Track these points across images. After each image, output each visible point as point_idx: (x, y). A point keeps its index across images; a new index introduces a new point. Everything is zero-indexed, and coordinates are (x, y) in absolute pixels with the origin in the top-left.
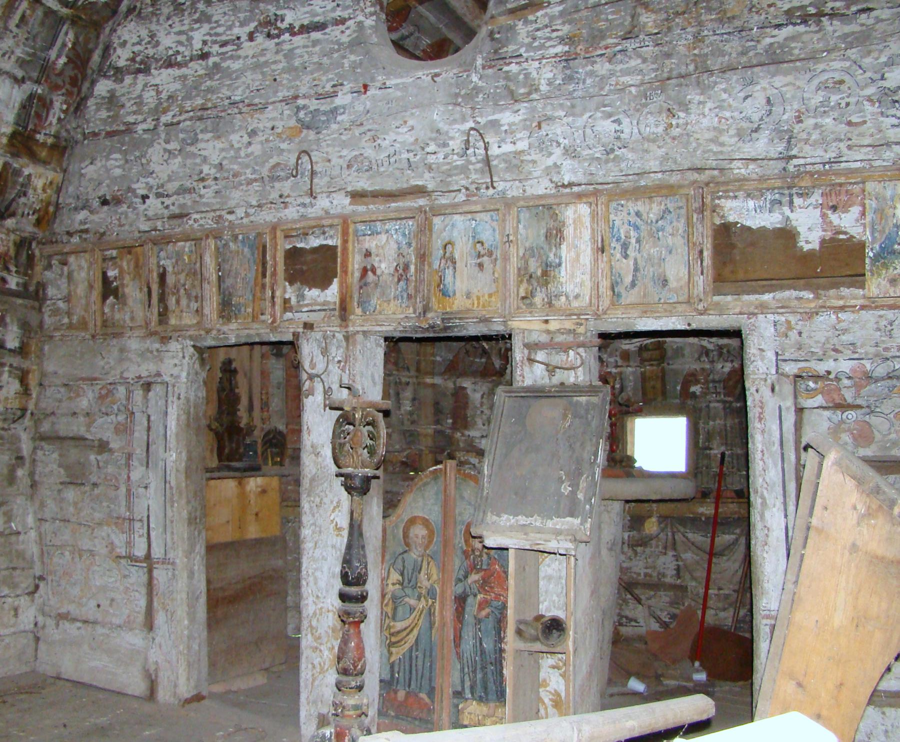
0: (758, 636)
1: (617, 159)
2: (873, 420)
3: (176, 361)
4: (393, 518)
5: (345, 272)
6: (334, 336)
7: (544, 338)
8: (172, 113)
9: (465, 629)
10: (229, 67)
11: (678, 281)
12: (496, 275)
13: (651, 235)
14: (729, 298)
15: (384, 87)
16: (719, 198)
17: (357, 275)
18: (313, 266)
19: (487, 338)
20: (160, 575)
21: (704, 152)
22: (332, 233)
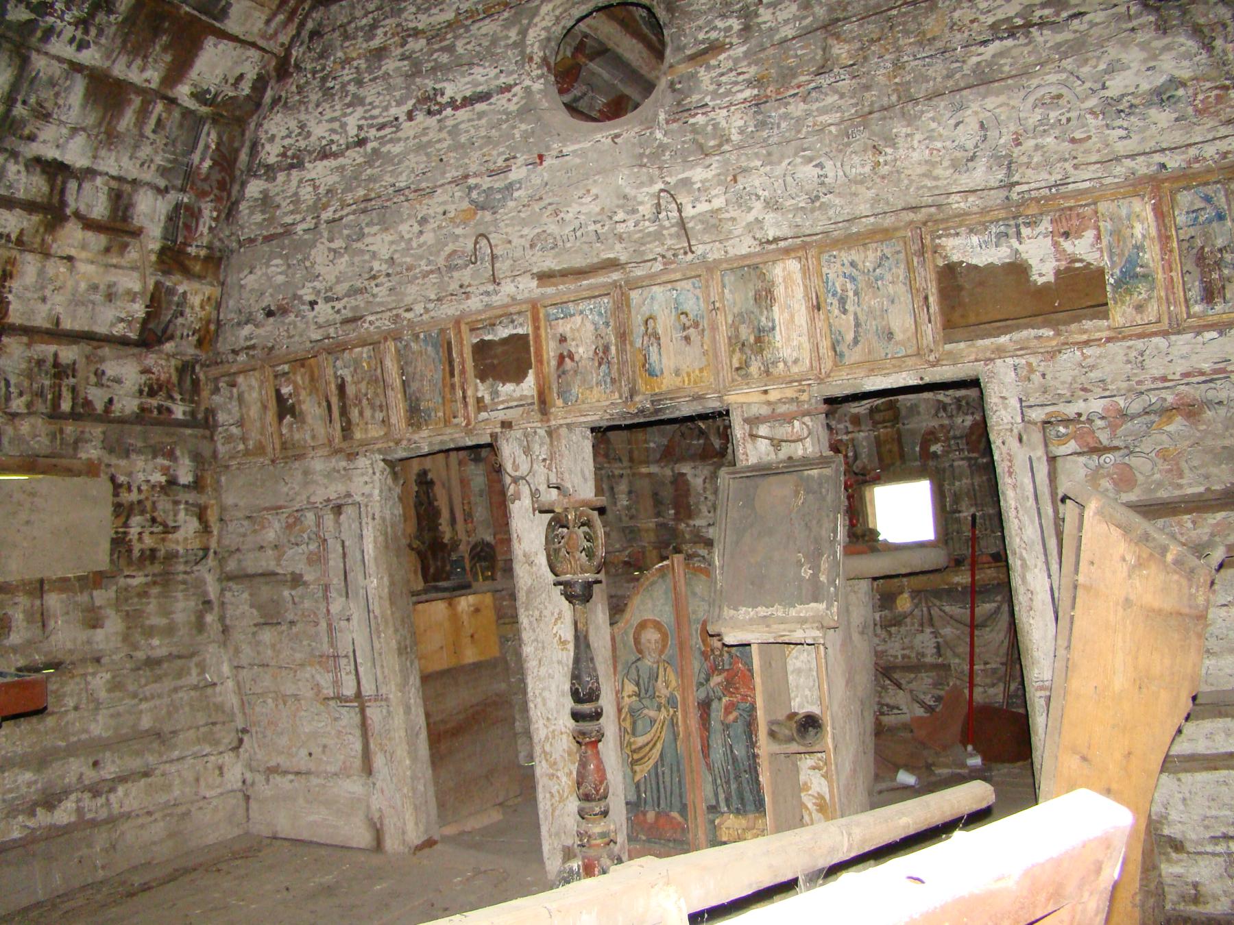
2: (1134, 461)
3: (366, 478)
4: (621, 624)
5: (540, 361)
7: (765, 411)
8: (333, 209)
9: (713, 737)
10: (389, 152)
11: (905, 331)
13: (870, 285)
14: (962, 345)
15: (561, 155)
16: (940, 237)
17: (554, 363)
18: (504, 359)
20: (374, 713)
21: (918, 189)
22: (521, 320)
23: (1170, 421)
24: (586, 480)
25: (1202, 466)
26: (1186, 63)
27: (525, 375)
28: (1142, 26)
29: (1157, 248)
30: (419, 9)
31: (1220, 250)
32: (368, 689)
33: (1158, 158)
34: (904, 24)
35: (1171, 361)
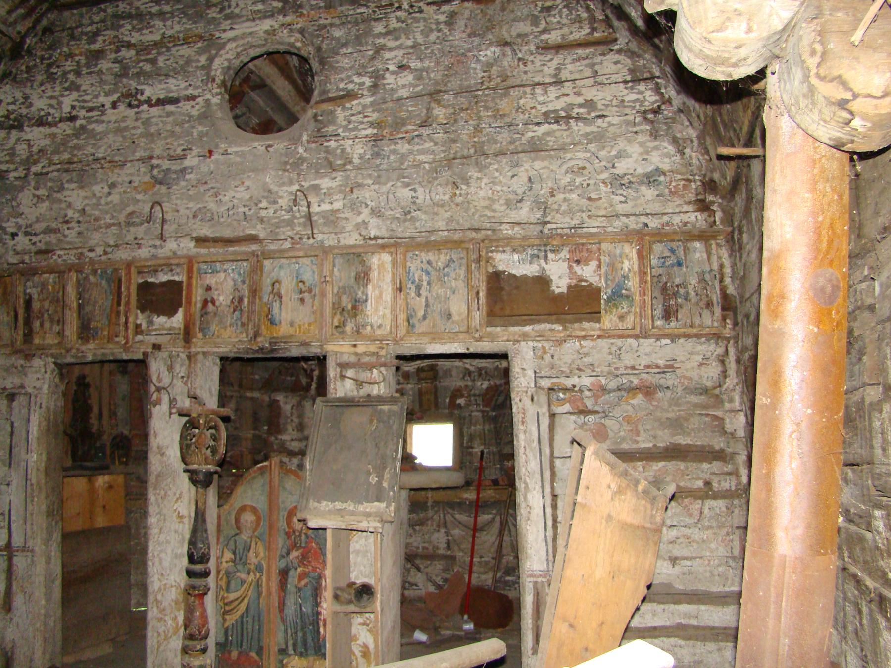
0: (524, 591)
1: (413, 220)
2: (608, 422)
3: (38, 375)
4: (226, 507)
5: (189, 302)
6: (178, 355)
7: (353, 359)
8: (42, 165)
9: (287, 597)
10: (93, 129)
11: (460, 315)
12: (315, 308)
13: (439, 279)
14: (499, 329)
15: (225, 153)
16: (492, 252)
17: (199, 305)
18: (162, 298)
19: (306, 359)
20: (20, 561)
21: (481, 216)
22: (178, 270)
23: (634, 397)
24: (211, 395)
25: (653, 429)
26: (667, 160)
27: (176, 312)
28: (642, 131)
29: (637, 279)
30: (134, 28)
31: (677, 286)
32: (17, 541)
33: (643, 219)
34: (486, 102)
35: (638, 356)
